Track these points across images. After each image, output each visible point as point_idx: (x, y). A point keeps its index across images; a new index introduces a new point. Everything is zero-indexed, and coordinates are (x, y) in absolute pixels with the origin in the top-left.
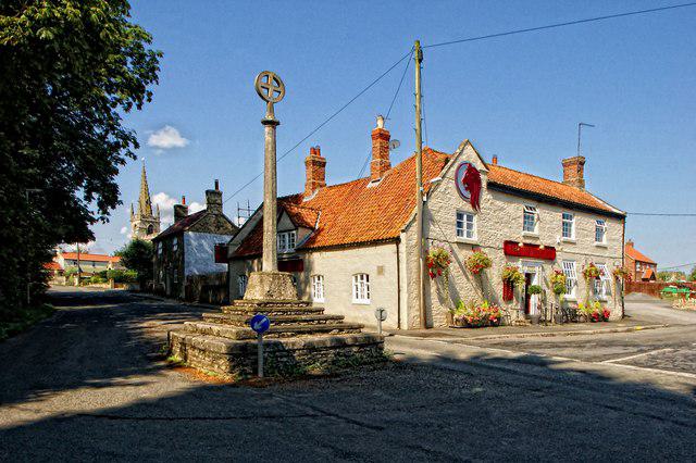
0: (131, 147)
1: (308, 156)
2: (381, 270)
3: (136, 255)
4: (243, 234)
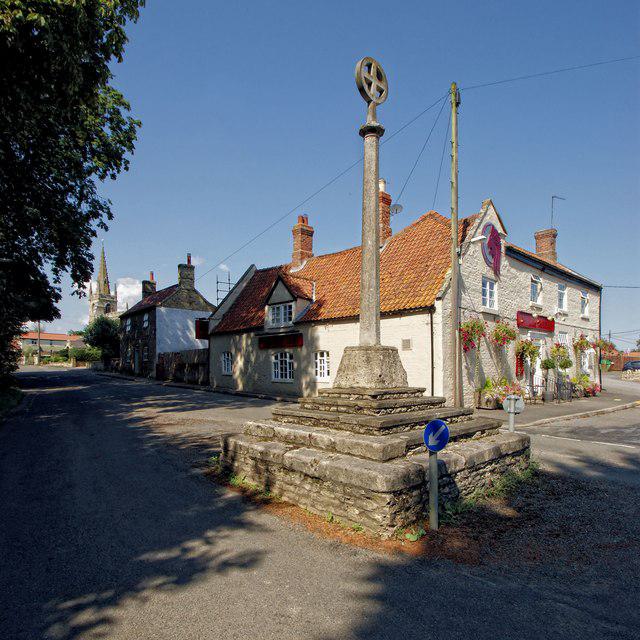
0: (105, 218)
1: (296, 224)
3: (101, 334)
4: (222, 311)
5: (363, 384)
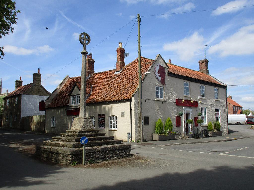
2: (123, 114)
5: (78, 129)
